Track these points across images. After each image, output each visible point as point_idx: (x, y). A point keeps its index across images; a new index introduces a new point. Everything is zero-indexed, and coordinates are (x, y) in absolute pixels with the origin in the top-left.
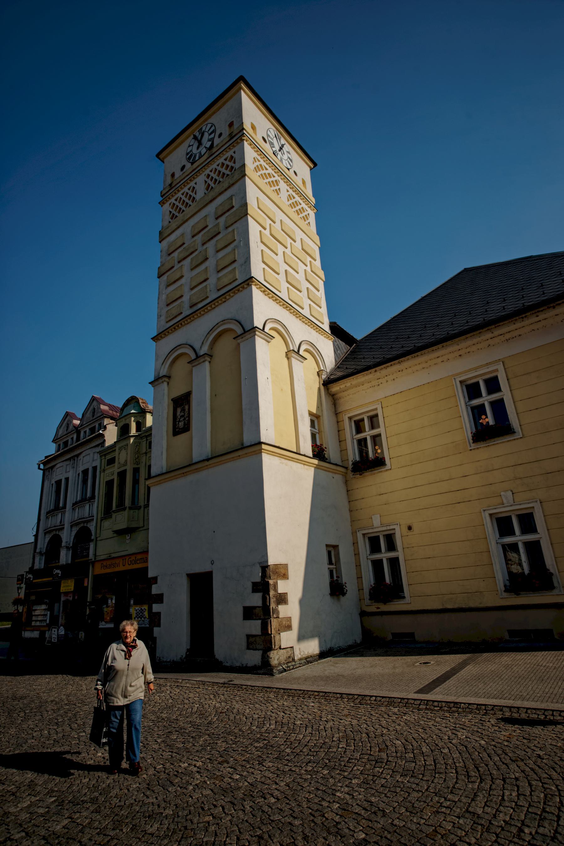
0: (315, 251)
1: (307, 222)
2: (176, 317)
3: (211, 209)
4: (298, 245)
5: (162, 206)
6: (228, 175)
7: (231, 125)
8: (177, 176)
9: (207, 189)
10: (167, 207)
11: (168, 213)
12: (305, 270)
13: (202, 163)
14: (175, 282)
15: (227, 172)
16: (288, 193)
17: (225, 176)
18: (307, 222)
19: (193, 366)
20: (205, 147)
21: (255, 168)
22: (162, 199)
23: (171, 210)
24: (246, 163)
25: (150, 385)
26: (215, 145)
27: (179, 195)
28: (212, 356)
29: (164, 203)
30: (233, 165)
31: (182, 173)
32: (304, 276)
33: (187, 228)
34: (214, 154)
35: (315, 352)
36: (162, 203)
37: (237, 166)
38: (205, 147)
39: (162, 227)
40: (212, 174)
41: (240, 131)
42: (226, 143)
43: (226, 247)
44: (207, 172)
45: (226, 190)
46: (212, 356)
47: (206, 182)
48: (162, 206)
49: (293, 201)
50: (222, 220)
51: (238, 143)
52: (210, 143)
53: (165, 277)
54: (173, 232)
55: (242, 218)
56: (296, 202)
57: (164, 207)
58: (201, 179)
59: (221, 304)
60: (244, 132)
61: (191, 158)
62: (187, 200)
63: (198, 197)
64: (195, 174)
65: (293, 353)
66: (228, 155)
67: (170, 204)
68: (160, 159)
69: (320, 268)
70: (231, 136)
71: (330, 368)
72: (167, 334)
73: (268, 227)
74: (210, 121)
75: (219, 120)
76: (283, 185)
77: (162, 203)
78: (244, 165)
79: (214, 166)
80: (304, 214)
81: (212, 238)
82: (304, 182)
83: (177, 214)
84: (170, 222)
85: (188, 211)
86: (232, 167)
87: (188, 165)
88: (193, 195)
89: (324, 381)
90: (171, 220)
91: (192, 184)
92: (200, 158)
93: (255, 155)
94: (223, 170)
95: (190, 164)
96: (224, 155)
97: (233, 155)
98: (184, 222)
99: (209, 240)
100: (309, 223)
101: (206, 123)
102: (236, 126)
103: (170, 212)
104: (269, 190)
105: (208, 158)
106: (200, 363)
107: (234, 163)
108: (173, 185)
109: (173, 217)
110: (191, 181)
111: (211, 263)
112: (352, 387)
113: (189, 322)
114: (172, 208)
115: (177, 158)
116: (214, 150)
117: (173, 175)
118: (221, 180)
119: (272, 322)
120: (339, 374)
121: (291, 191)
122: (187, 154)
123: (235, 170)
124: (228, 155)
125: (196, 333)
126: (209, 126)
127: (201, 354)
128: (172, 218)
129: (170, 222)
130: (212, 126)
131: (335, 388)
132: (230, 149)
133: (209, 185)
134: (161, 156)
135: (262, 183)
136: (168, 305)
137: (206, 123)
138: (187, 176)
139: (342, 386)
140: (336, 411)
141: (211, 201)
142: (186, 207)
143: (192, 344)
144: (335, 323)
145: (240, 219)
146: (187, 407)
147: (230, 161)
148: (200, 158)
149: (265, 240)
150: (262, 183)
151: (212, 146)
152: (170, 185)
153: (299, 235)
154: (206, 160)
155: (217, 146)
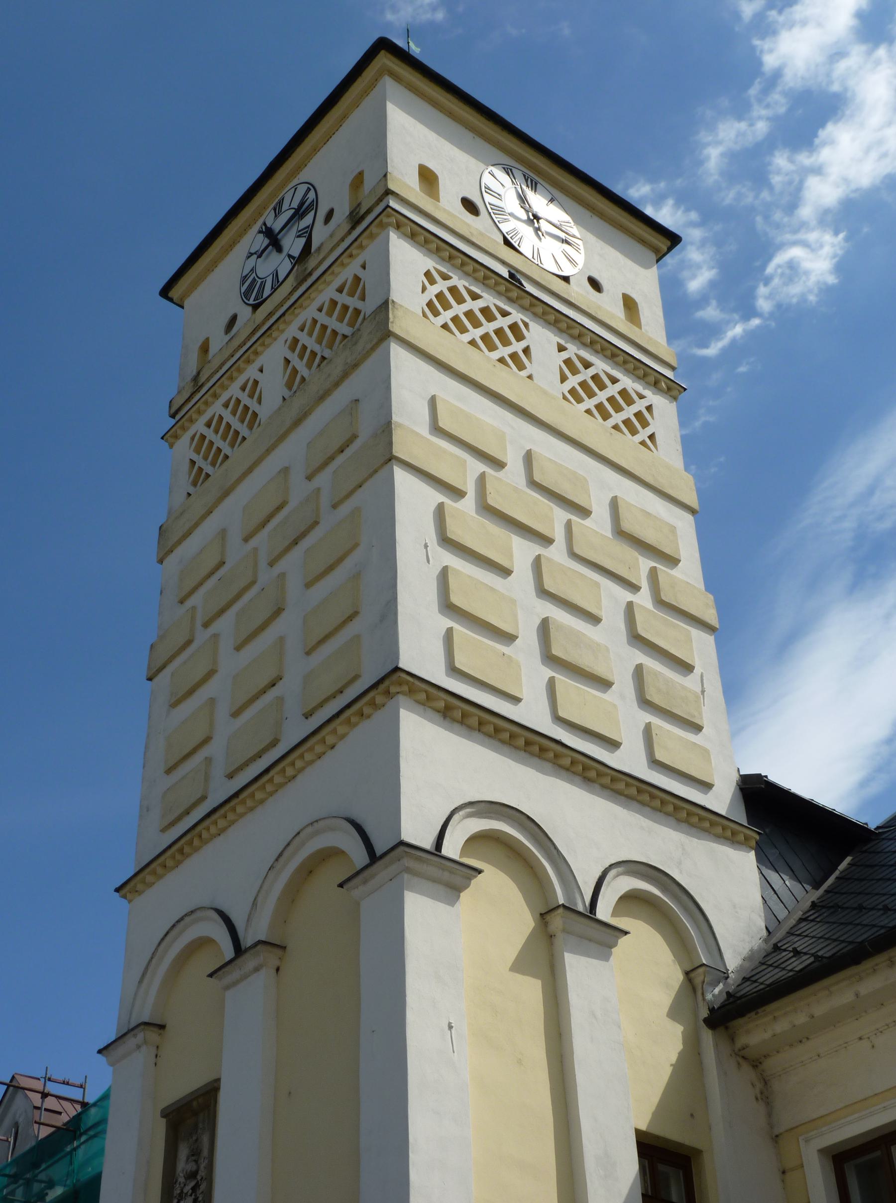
0: (673, 529)
1: (643, 434)
2: (187, 812)
3: (294, 450)
4: (599, 523)
5: (171, 446)
6: (345, 337)
7: (358, 180)
8: (213, 349)
9: (289, 385)
10: (184, 448)
11: (186, 465)
12: (630, 606)
13: (281, 305)
14: (191, 692)
15: (344, 329)
16: (565, 355)
17: (339, 338)
18: (643, 434)
19: (227, 988)
20: (290, 256)
21: (430, 304)
22: (173, 421)
23: (195, 457)
24: (395, 296)
25: (100, 1055)
26: (315, 245)
27: (217, 408)
28: (284, 948)
29: (176, 437)
30: (359, 305)
31: (228, 337)
32: (622, 626)
33: (231, 514)
34: (310, 274)
35: (666, 903)
36: (170, 437)
37: (368, 307)
38: (290, 256)
39: (170, 513)
40: (304, 338)
41: (380, 200)
42: (342, 240)
43: (331, 568)
44: (292, 330)
45: (337, 384)
46: (284, 948)
47: (287, 361)
48: (171, 446)
49: (586, 375)
50: (323, 479)
51: (372, 237)
52: (303, 241)
53: (164, 678)
54: (196, 525)
55: (376, 471)
56: (595, 378)
57: (176, 447)
58: (274, 354)
59: (312, 762)
60: (393, 203)
61: (253, 292)
62: (236, 424)
63: (264, 412)
64: (263, 334)
65: (564, 925)
66: (345, 274)
67: (193, 438)
68: (171, 300)
69: (701, 585)
70: (355, 219)
71: (745, 950)
72: (160, 870)
73: (471, 489)
74: (304, 176)
75: (325, 172)
76: (541, 338)
77: (170, 437)
78: (385, 305)
79: (308, 313)
80: (629, 412)
81: (295, 542)
82: (630, 305)
83: (208, 469)
84: (189, 494)
85: (239, 456)
86: (357, 312)
87: (245, 313)
88: (253, 405)
89: (712, 1010)
90: (191, 490)
91: (251, 372)
92: (274, 289)
93: (428, 263)
94: (333, 323)
95: (250, 309)
96: (335, 275)
97: (361, 273)
98: (226, 494)
99: (288, 549)
100: (652, 437)
101: (295, 182)
102: (369, 183)
103: (193, 463)
104: (483, 365)
105: (295, 289)
106: (245, 977)
107: (363, 298)
108: (202, 379)
109: (199, 477)
110: (248, 362)
111: (288, 625)
112: (801, 1038)
113: (224, 830)
114: (197, 451)
115: (218, 291)
116: (312, 263)
117: (205, 348)
118: (327, 353)
119: (469, 816)
120: (771, 976)
121: (573, 350)
122: (244, 279)
123: (364, 319)
124: (345, 274)
125: (234, 870)
126: (302, 189)
127: (249, 945)
128: (195, 484)
129: (189, 494)
130: (309, 189)
131: (757, 1032)
132: (351, 256)
133: (295, 371)
134: (175, 293)
135: (455, 348)
136: (169, 771)
137: (295, 182)
138: (240, 346)
139: (801, 1019)
140: (771, 1126)
141: (297, 422)
142: (232, 445)
143: (225, 908)
144: (758, 779)
145: (371, 476)
146: (205, 1139)
147: (352, 294)
148: (274, 289)
149: (455, 531)
150: (455, 348)
151: (307, 250)
152: (196, 379)
153: (600, 487)
154: (291, 293)
155: (319, 249)
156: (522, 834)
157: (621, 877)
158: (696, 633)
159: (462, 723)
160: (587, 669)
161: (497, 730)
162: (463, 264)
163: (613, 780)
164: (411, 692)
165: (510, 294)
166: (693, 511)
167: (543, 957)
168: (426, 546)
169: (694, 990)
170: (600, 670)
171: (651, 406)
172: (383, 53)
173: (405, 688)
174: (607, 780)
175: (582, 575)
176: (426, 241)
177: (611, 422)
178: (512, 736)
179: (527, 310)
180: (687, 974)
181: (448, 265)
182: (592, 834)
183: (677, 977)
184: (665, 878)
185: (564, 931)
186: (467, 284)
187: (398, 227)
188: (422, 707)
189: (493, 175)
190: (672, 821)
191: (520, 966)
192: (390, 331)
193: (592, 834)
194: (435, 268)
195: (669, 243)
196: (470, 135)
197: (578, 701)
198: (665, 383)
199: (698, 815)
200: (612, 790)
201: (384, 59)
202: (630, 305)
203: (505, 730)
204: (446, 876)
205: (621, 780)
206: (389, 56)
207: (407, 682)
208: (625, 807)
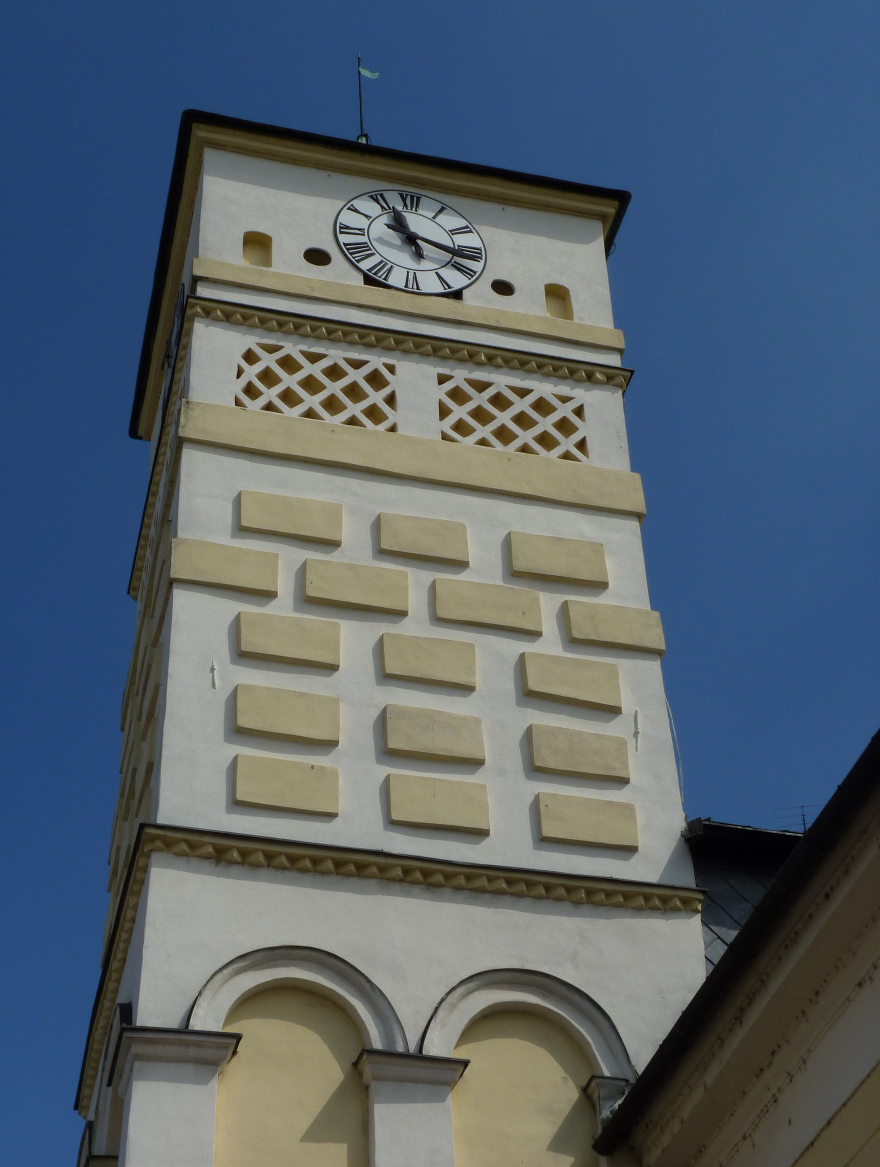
68: (140, 438)
69: (645, 604)
82: (557, 294)
134: (141, 431)
156: (321, 974)
157: (476, 993)
158: (626, 665)
159: (243, 863)
160: (441, 753)
161: (293, 859)
162: (297, 327)
163: (469, 878)
164: (168, 845)
165: (366, 340)
166: (638, 516)
167: (350, 1116)
168: (212, 670)
169: (594, 1107)
170: (461, 749)
171: (582, 407)
172: (195, 126)
173: (159, 844)
174: (462, 881)
175: (445, 641)
176: (245, 318)
177: (517, 443)
178: (315, 861)
179: (394, 350)
180: (585, 1090)
181: (279, 334)
182: (420, 956)
183: (573, 1094)
184: (545, 980)
185: (375, 1078)
186: (305, 348)
187: (207, 313)
188: (184, 859)
189: (356, 211)
190: (566, 906)
191: (317, 1132)
192: (180, 438)
193: (420, 956)
194: (259, 345)
195: (616, 203)
196: (323, 174)
197: (427, 793)
198: (602, 373)
199: (603, 890)
200: (471, 890)
201: (200, 132)
202: (557, 294)
203: (303, 857)
204: (192, 1052)
205: (480, 876)
206: (202, 126)
207: (159, 837)
208: (489, 905)
